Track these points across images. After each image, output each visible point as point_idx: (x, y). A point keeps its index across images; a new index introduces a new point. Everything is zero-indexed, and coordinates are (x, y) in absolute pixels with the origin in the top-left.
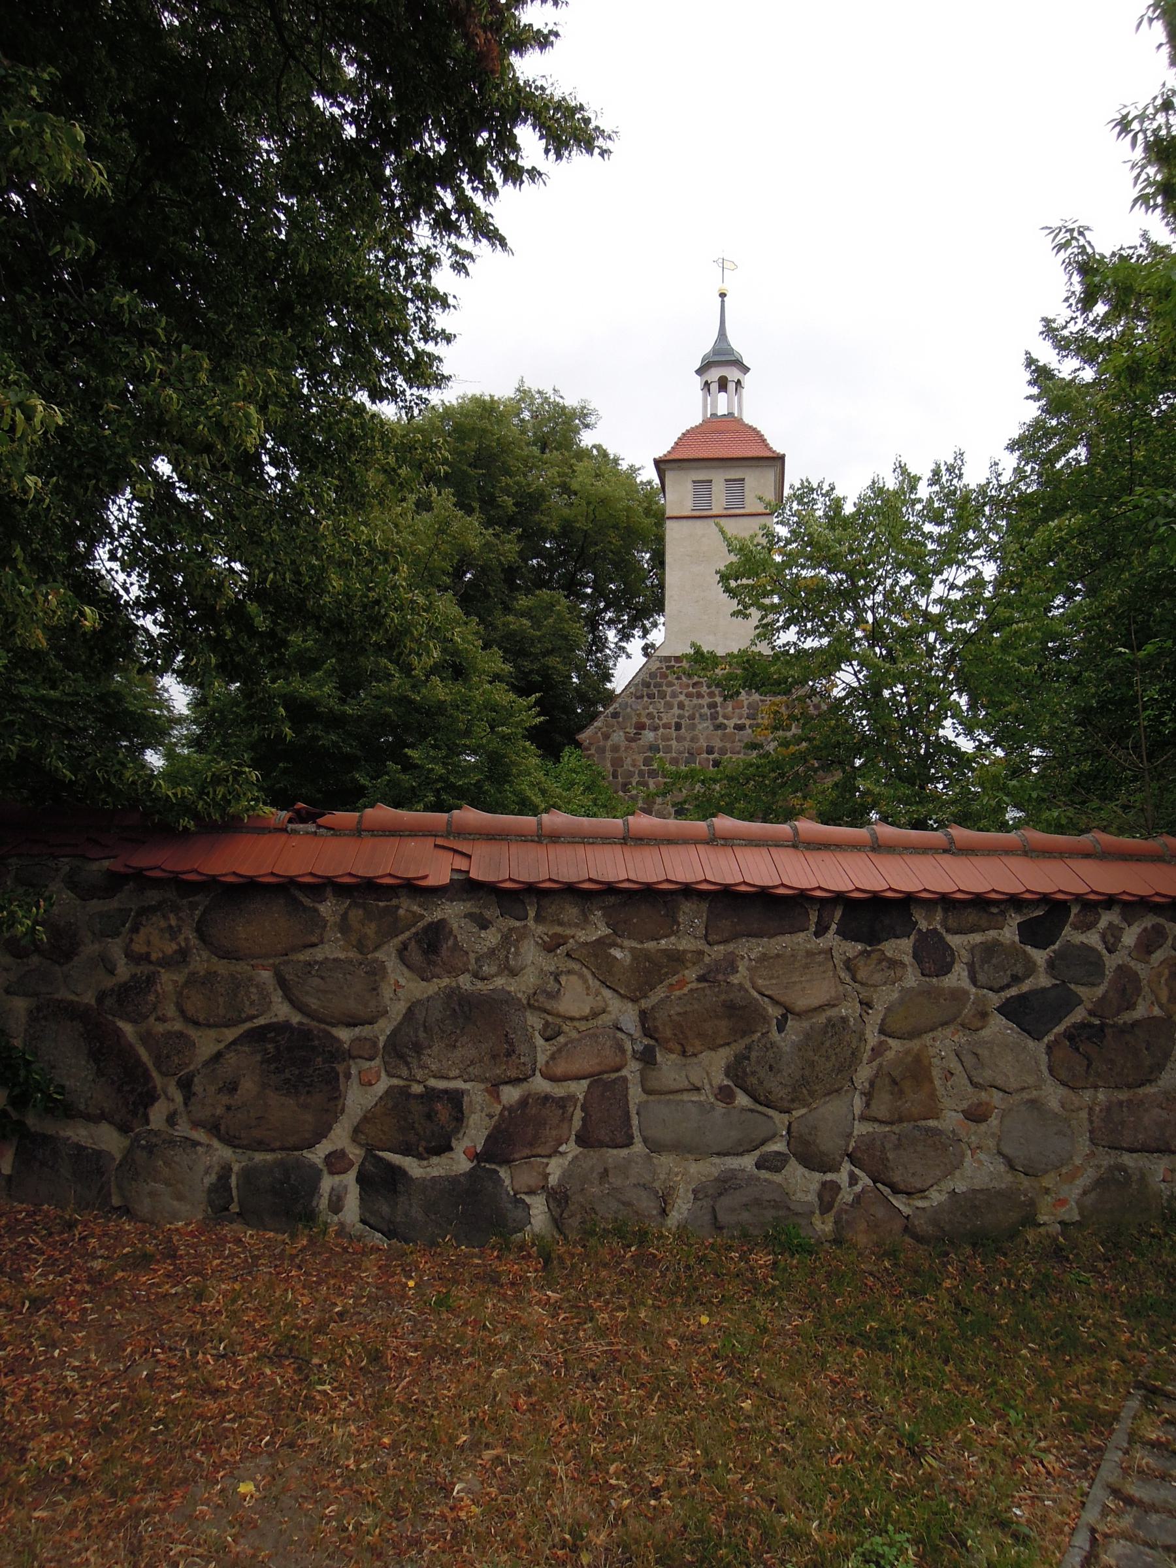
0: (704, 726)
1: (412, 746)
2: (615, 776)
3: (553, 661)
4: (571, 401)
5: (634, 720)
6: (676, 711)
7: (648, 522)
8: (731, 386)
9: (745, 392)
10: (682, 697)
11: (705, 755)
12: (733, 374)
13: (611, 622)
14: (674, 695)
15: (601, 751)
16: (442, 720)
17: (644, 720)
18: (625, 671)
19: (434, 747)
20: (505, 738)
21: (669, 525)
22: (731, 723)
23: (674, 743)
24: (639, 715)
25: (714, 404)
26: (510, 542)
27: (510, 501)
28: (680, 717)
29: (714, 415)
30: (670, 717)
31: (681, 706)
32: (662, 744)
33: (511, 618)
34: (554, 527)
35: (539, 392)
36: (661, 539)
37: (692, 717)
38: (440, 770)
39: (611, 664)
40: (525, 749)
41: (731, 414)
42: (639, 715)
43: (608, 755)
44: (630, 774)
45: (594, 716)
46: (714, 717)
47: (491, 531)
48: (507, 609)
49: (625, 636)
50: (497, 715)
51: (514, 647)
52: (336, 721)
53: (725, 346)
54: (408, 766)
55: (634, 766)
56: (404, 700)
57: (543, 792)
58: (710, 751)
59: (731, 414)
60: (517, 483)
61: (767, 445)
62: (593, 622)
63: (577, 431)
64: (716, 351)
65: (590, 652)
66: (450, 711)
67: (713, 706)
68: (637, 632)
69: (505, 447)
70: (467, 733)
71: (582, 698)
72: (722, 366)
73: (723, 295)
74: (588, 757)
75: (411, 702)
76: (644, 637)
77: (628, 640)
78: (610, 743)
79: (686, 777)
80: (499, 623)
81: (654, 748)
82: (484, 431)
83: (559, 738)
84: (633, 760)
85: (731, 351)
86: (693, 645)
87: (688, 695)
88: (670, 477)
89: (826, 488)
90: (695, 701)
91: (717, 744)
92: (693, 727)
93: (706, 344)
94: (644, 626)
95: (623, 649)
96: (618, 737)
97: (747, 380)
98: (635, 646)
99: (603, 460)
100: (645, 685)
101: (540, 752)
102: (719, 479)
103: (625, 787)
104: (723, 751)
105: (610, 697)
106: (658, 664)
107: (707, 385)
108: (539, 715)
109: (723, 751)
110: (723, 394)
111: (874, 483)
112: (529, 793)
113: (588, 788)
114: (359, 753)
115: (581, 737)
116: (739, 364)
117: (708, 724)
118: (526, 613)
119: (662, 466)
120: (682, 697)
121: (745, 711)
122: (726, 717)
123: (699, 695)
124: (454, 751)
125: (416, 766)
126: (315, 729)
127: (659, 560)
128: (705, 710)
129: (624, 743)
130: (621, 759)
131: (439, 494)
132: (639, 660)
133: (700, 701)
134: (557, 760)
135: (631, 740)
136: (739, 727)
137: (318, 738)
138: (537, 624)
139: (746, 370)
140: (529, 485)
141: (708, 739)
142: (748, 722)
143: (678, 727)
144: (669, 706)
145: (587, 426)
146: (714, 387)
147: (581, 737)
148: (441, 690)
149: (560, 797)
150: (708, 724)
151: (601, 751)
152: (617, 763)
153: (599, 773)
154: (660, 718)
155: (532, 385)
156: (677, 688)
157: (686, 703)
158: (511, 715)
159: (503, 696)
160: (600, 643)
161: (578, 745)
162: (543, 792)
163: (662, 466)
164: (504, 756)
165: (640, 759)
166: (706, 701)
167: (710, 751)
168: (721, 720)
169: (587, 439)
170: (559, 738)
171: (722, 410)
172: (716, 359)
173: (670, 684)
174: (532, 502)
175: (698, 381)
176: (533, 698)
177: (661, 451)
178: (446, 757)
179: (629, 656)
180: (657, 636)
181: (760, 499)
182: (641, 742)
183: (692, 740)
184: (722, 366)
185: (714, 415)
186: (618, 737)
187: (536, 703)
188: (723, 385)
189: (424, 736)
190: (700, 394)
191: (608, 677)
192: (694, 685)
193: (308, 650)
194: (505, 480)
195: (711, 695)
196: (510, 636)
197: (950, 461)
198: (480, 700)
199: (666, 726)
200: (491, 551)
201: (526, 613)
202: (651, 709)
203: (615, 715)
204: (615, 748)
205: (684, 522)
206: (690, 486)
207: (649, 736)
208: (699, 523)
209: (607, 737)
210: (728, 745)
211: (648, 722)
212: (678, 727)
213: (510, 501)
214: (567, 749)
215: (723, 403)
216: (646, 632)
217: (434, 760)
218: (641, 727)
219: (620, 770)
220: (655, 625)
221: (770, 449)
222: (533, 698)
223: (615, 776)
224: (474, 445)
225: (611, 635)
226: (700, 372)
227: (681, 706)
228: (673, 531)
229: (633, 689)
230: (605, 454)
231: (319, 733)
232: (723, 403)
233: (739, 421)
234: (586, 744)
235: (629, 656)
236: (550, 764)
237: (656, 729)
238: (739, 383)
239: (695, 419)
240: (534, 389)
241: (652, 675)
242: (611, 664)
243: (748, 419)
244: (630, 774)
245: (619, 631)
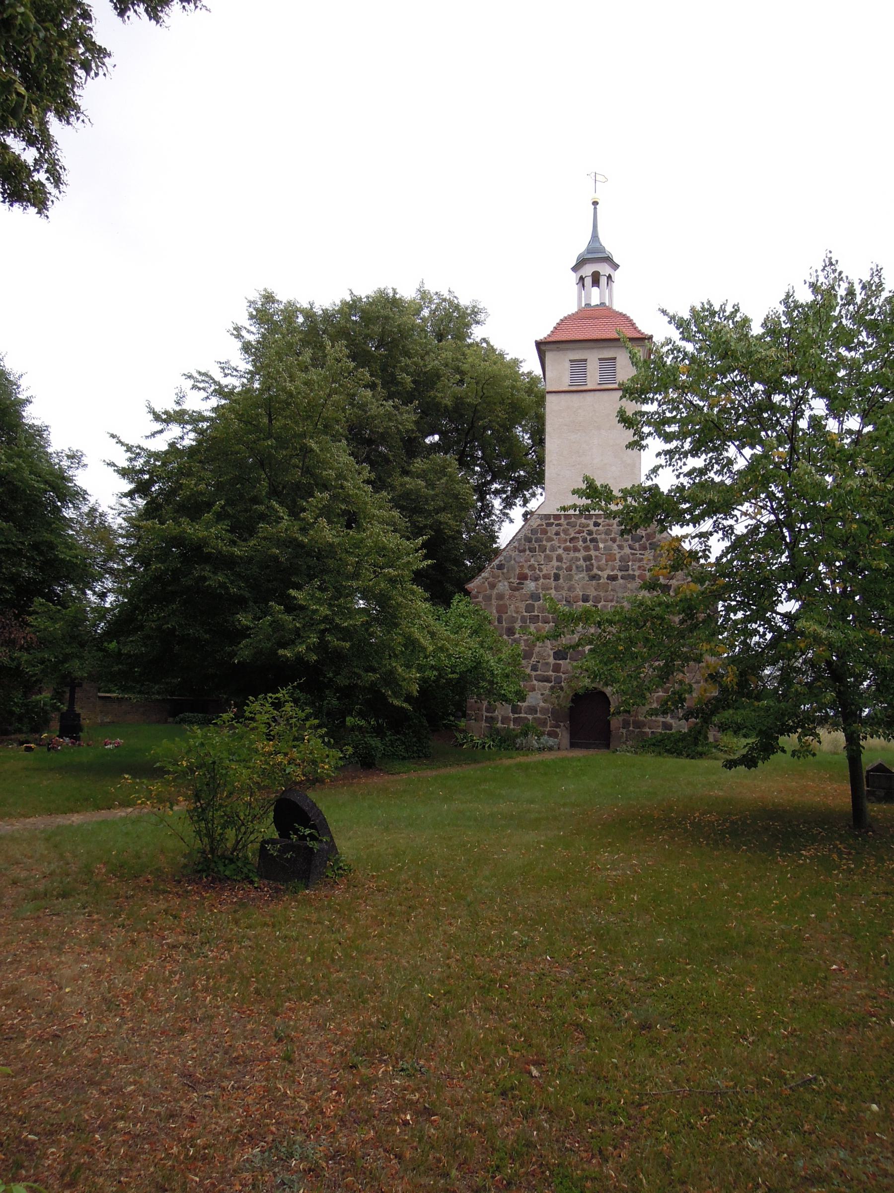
0: (580, 577)
1: (299, 587)
2: (500, 621)
3: (444, 517)
4: (464, 301)
5: (517, 572)
6: (555, 563)
7: (529, 399)
8: (603, 280)
9: (615, 286)
10: (560, 551)
11: (581, 603)
12: (604, 269)
13: (497, 493)
14: (553, 549)
15: (488, 598)
16: (331, 563)
17: (527, 571)
18: (507, 534)
19: (320, 588)
20: (392, 581)
21: (550, 399)
22: (604, 574)
23: (553, 592)
24: (522, 567)
25: (588, 296)
26: (408, 412)
27: (409, 379)
28: (558, 568)
29: (588, 305)
30: (549, 569)
31: (559, 559)
32: (542, 593)
33: (407, 479)
34: (448, 402)
35: (437, 293)
36: (540, 420)
37: (569, 569)
38: (324, 611)
39: (496, 528)
40: (413, 593)
41: (602, 304)
42: (522, 567)
43: (494, 602)
44: (513, 620)
45: (481, 569)
46: (589, 569)
47: (391, 403)
48: (406, 473)
49: (508, 504)
50: (391, 557)
51: (409, 504)
52: (225, 562)
53: (597, 245)
54: (291, 607)
55: (517, 612)
56: (292, 543)
57: (433, 634)
58: (585, 599)
59: (602, 304)
60: (415, 364)
61: (636, 328)
62: (482, 491)
63: (468, 326)
64: (589, 250)
65: (479, 517)
66: (340, 554)
67: (588, 558)
68: (519, 501)
69: (404, 333)
70: (356, 576)
71: (472, 553)
72: (594, 265)
73: (595, 203)
74: (476, 604)
75: (301, 545)
76: (524, 505)
77: (510, 508)
78: (495, 591)
79: (579, 619)
80: (396, 483)
81: (535, 597)
82: (387, 318)
83: (450, 588)
84: (516, 608)
85: (603, 250)
86: (586, 479)
87: (566, 549)
88: (549, 357)
89: (729, 309)
90: (572, 554)
91: (592, 593)
92: (570, 578)
93: (581, 246)
94: (524, 496)
95: (506, 515)
96: (503, 587)
97: (617, 275)
98: (517, 512)
99: (490, 353)
100: (528, 541)
101: (427, 595)
102: (593, 358)
103: (511, 632)
104: (597, 600)
105: (497, 552)
106: (539, 522)
107: (582, 279)
108: (426, 557)
109: (597, 600)
110: (595, 289)
111: (788, 296)
112: (417, 635)
113: (475, 632)
114: (247, 595)
115: (470, 586)
116: (608, 260)
117: (583, 574)
118: (423, 475)
119: (543, 347)
120: (560, 551)
121: (617, 563)
122: (599, 568)
123: (576, 550)
124: (340, 592)
125: (302, 608)
126: (203, 570)
127: (539, 439)
128: (581, 562)
129: (508, 592)
130: (505, 606)
131: (333, 346)
132: (519, 523)
133: (577, 554)
134: (448, 605)
135: (516, 589)
136: (613, 578)
137: (205, 579)
138: (431, 485)
139: (616, 266)
140: (425, 366)
141: (583, 588)
142: (620, 574)
143: (557, 577)
144: (549, 559)
145: (478, 323)
146: (588, 281)
147: (470, 586)
148: (328, 533)
149: (448, 639)
150: (583, 574)
151: (488, 598)
152: (502, 609)
153: (486, 618)
154: (541, 570)
155: (432, 287)
156: (556, 543)
157: (564, 556)
158: (398, 558)
159: (392, 540)
160: (487, 510)
161: (467, 593)
162: (433, 634)
163: (543, 347)
164: (390, 599)
165: (522, 606)
166: (582, 554)
167: (585, 599)
168: (595, 571)
169: (477, 333)
170: (450, 588)
171: (595, 301)
172: (589, 256)
173: (550, 539)
174: (427, 381)
175: (573, 277)
176: (420, 541)
177: (543, 334)
178: (331, 599)
179: (511, 521)
180: (533, 505)
181: (664, 312)
182: (524, 592)
183: (569, 589)
184: (594, 265)
185: (588, 305)
186: (503, 587)
187: (424, 545)
188: (596, 280)
189: (311, 578)
190: (575, 288)
191: (493, 538)
192: (572, 540)
193: (201, 493)
194: (404, 361)
195: (587, 549)
196: (406, 495)
197: (866, 278)
198: (369, 543)
199: (546, 577)
200: (390, 420)
201: (423, 475)
202: (532, 561)
203: (500, 567)
204: (500, 597)
205: (563, 395)
206: (567, 365)
207: (531, 585)
208: (575, 397)
209: (493, 586)
210: (602, 594)
211: (530, 573)
212: (557, 577)
213: (409, 379)
214: (457, 596)
215: (595, 296)
216: (526, 502)
217: (319, 601)
218: (523, 577)
219: (504, 616)
220: (534, 495)
221: (639, 331)
222: (420, 541)
223: (500, 621)
224: (377, 329)
225: (497, 503)
226: (575, 269)
227: (559, 559)
228: (553, 407)
229: (516, 544)
230: (492, 349)
231: (206, 574)
232: (595, 296)
233: (609, 308)
234: (474, 592)
235: (511, 521)
236: (441, 610)
237: (536, 579)
238: (609, 277)
239: (572, 308)
240: (433, 291)
241: (534, 531)
242: (496, 528)
243: (618, 307)
244: (513, 620)
245: (504, 500)
